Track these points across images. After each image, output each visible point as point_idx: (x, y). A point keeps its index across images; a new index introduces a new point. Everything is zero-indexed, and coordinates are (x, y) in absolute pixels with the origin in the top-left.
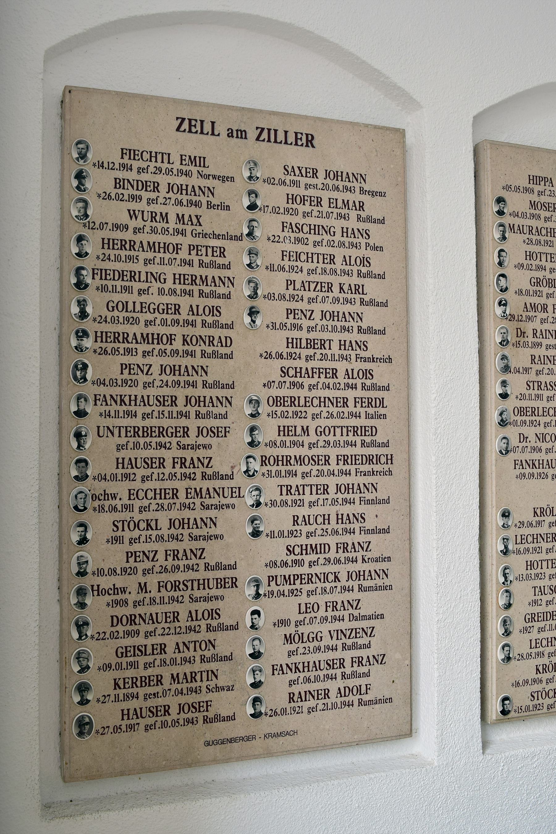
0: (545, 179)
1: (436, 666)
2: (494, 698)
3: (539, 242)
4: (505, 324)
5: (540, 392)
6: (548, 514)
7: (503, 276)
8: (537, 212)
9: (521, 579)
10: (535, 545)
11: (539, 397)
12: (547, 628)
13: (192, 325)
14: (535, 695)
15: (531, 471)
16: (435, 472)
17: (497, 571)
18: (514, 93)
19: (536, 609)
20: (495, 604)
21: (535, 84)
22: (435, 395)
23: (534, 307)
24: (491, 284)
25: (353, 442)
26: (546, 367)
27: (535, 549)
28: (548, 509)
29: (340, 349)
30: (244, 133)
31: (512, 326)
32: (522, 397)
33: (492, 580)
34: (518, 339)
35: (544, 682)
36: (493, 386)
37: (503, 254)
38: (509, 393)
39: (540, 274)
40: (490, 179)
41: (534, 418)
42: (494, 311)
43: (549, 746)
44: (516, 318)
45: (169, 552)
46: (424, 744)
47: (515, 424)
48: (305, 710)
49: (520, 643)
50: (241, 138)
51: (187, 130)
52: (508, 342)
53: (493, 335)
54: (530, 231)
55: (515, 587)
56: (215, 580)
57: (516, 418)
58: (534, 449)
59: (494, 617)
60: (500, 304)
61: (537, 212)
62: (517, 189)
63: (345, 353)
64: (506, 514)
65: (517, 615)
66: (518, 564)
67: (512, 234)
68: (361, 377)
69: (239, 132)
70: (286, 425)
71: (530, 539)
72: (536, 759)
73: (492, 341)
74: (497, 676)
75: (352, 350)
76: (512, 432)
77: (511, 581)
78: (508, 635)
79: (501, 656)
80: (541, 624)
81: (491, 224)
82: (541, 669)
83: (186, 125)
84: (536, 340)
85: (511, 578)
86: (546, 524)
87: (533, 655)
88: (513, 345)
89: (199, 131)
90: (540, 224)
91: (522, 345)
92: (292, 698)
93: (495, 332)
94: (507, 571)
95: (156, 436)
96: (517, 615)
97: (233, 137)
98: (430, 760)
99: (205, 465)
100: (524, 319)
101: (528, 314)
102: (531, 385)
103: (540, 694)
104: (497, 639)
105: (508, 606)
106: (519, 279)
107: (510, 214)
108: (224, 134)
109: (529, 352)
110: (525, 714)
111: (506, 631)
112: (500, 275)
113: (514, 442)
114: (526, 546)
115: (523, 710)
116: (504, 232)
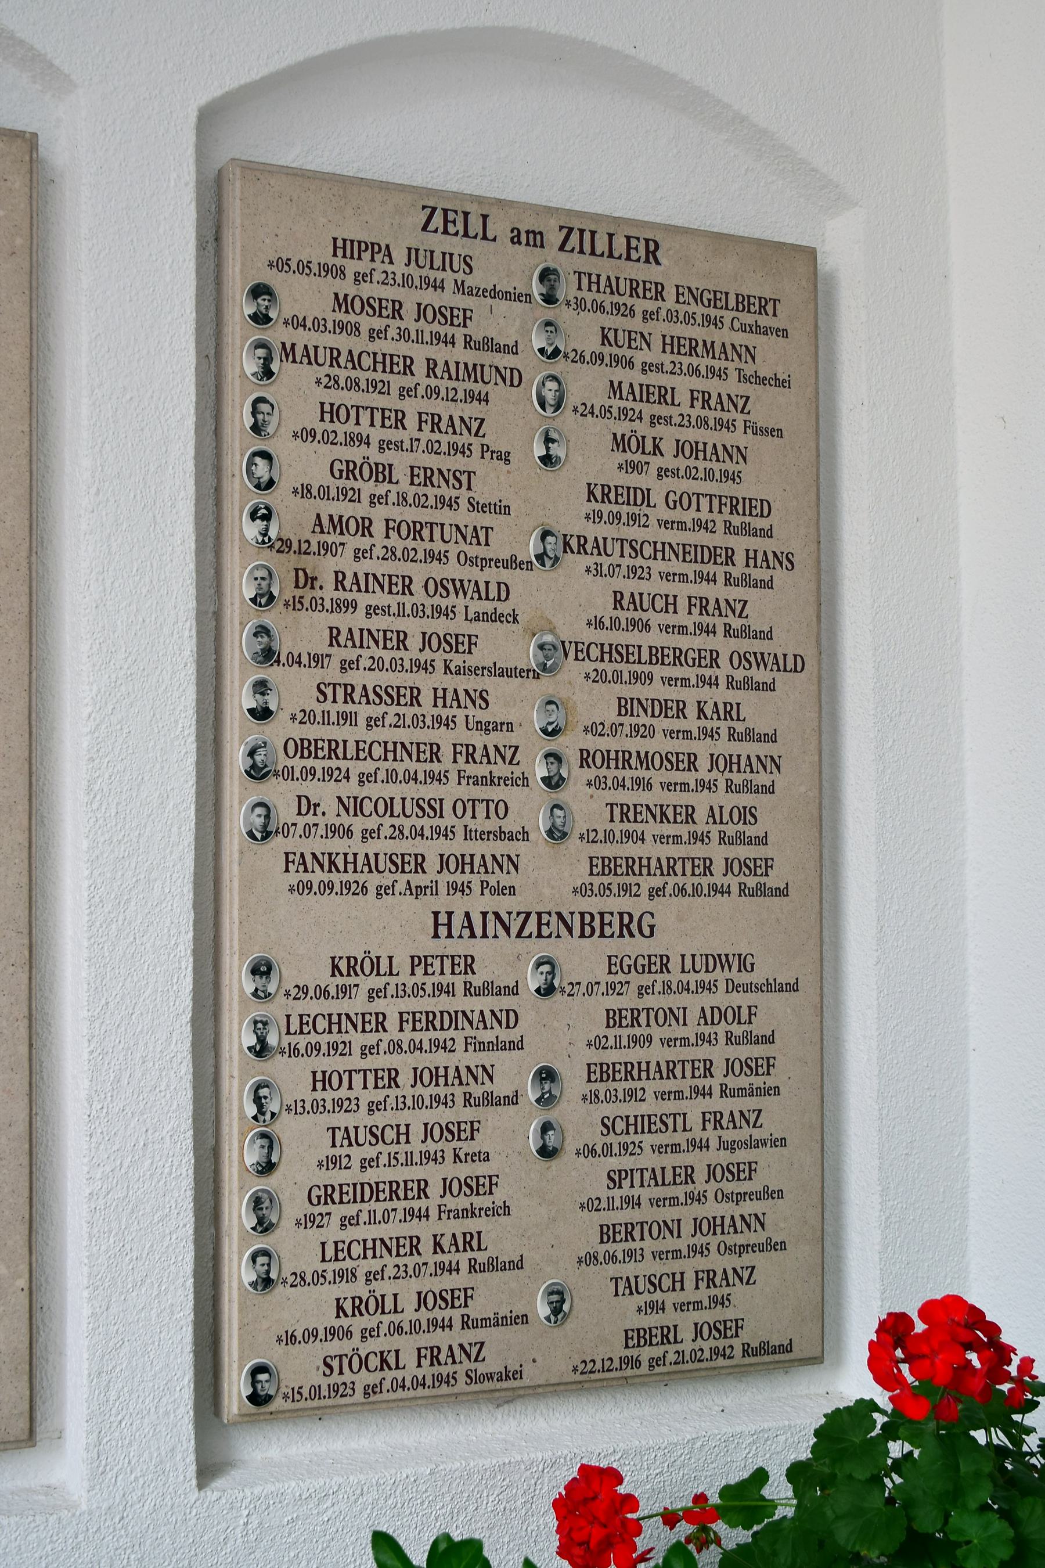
0: (373, 248)
1: (86, 1294)
2: (235, 1366)
3: (353, 385)
4: (269, 558)
5: (350, 708)
6: (367, 971)
7: (266, 455)
8: (352, 318)
9: (300, 1110)
10: (335, 1037)
11: (347, 718)
12: (364, 1217)
14: (335, 1364)
15: (326, 877)
16: (87, 873)
17: (241, 1091)
18: (301, 57)
19: (337, 1177)
20: (236, 1164)
21: (353, 39)
22: (89, 709)
23: (339, 524)
24: (237, 473)
26: (366, 653)
27: (334, 1047)
28: (367, 962)
29: (435, 705)
30: (538, 237)
31: (283, 565)
32: (307, 717)
33: (230, 1111)
34: (298, 593)
35: (357, 1336)
36: (237, 692)
37: (264, 407)
38: (273, 707)
39: (356, 454)
40: (238, 244)
41: (334, 763)
42: (241, 530)
43: (362, 1477)
44: (295, 546)
46: (66, 1467)
47: (288, 774)
49: (296, 1248)
50: (535, 245)
51: (441, 229)
52: (271, 598)
53: (237, 582)
54: (334, 361)
55: (286, 1128)
57: (290, 763)
58: (333, 830)
59: (235, 1191)
60: (253, 516)
61: (352, 318)
62: (304, 267)
63: (445, 713)
64: (262, 969)
65: (292, 1185)
66: (292, 1077)
67: (288, 366)
68: (736, 820)
69: (531, 236)
71: (322, 1024)
72: (329, 1503)
73: (237, 594)
74: (240, 1321)
75: (459, 706)
76: (282, 796)
77: (273, 1114)
78: (266, 1230)
79: (249, 1276)
80: (351, 1210)
81: (238, 342)
82: (348, 1306)
83: (438, 221)
84: (341, 595)
85: (273, 1106)
86: (362, 994)
87: (330, 1276)
88: (287, 604)
89: (461, 233)
90: (358, 344)
91: (307, 604)
93: (241, 576)
94: (264, 1092)
96: (292, 1185)
97: (519, 243)
98: (76, 1498)
100: (314, 548)
101: (324, 538)
102: (329, 691)
103: (345, 1361)
104: (242, 1239)
105: (267, 1168)
106: (304, 463)
107: (286, 323)
108: (505, 237)
109: (324, 620)
110: (310, 1404)
111: (260, 1221)
112: (255, 454)
113: (286, 812)
114: (313, 1038)
115: (306, 1394)
116: (268, 360)
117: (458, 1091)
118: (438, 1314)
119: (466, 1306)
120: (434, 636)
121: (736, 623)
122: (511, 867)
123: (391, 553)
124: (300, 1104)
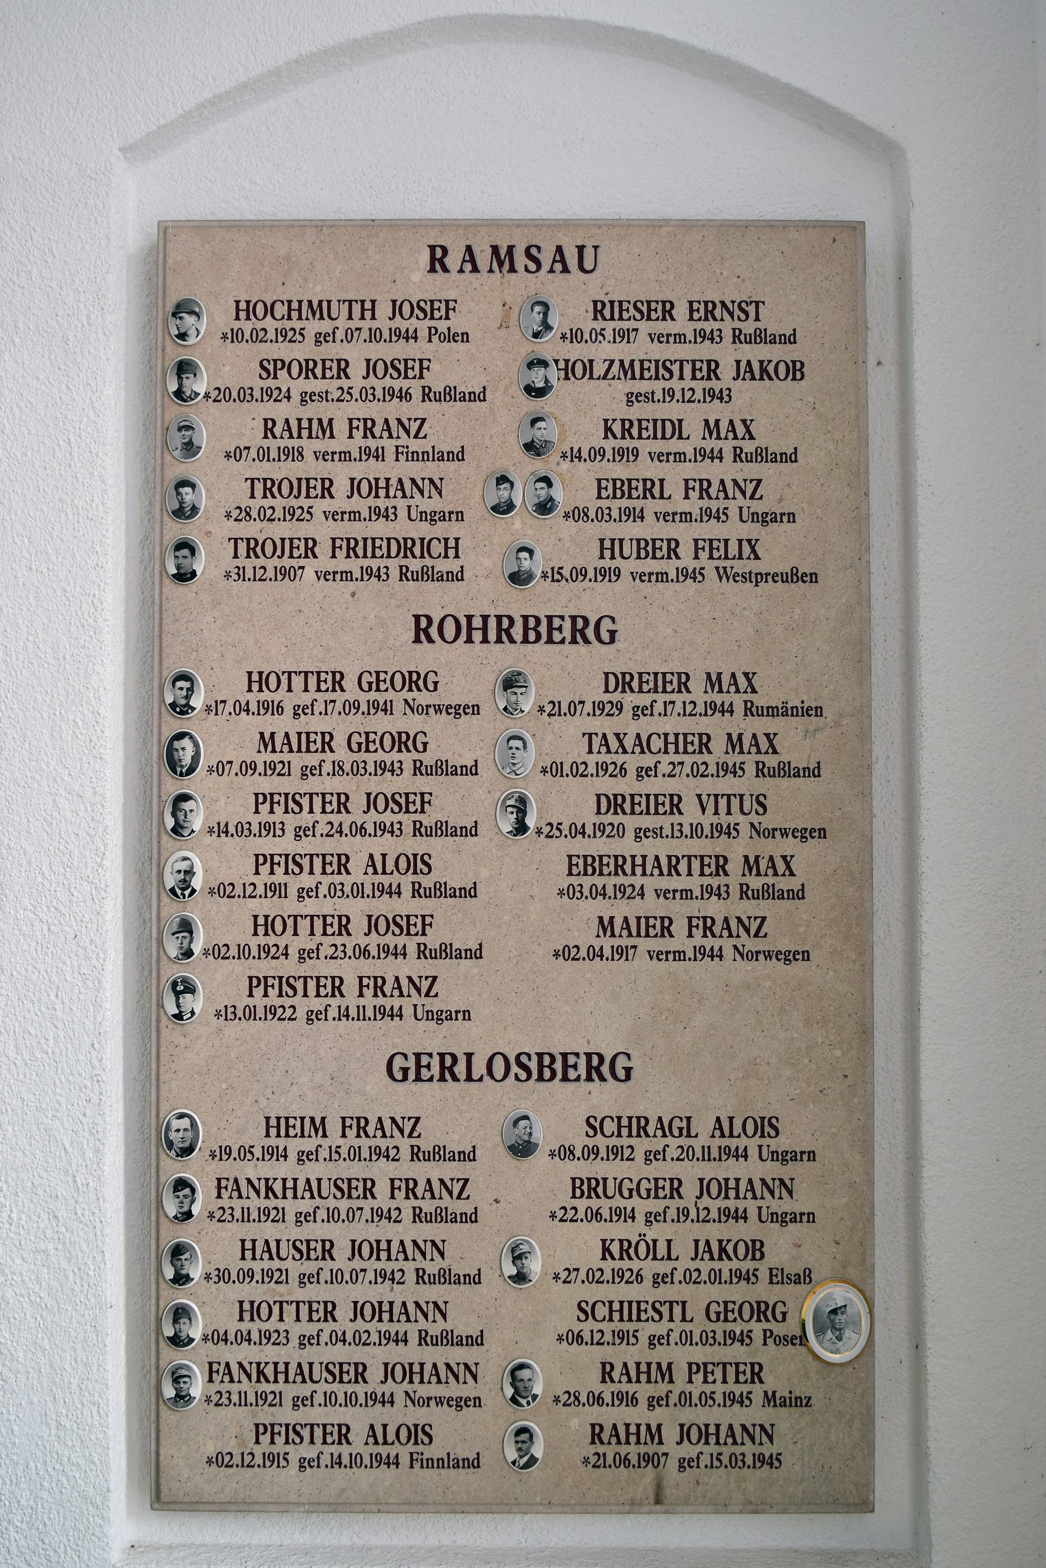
9: (230, 1016)
13: (377, 457)
15: (263, 1203)
25: (400, 947)
27: (268, 1274)
45: (355, 423)
48: (301, 1014)
56: (635, 543)
70: (369, 535)
92: (271, 430)
95: (702, 378)
99: (424, 991)
117: (410, 1267)
118: (390, 940)
119: (424, 934)
120: (382, 919)
121: (750, 944)
122: (469, 1376)
123: (329, 1399)
124: (230, 1010)
